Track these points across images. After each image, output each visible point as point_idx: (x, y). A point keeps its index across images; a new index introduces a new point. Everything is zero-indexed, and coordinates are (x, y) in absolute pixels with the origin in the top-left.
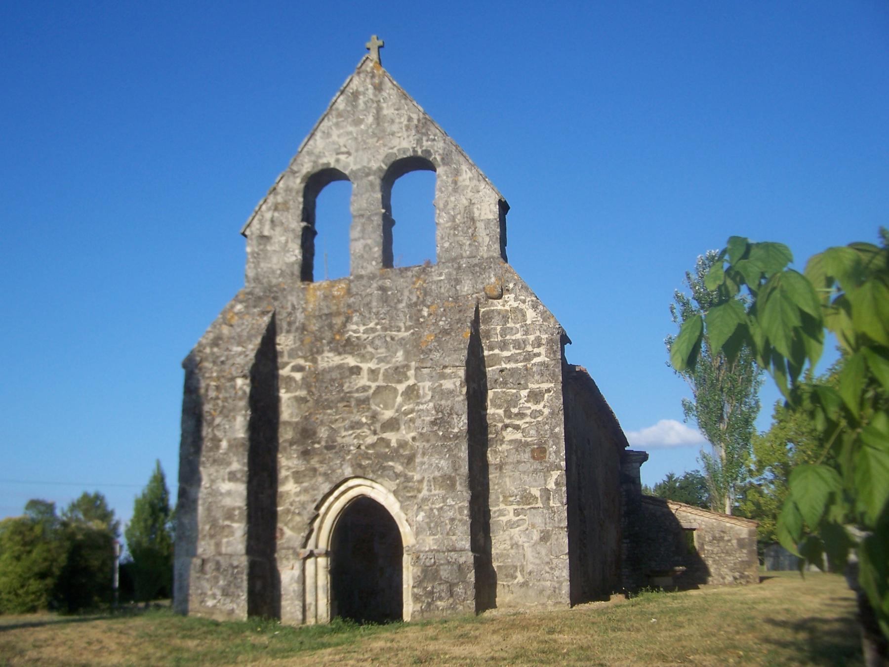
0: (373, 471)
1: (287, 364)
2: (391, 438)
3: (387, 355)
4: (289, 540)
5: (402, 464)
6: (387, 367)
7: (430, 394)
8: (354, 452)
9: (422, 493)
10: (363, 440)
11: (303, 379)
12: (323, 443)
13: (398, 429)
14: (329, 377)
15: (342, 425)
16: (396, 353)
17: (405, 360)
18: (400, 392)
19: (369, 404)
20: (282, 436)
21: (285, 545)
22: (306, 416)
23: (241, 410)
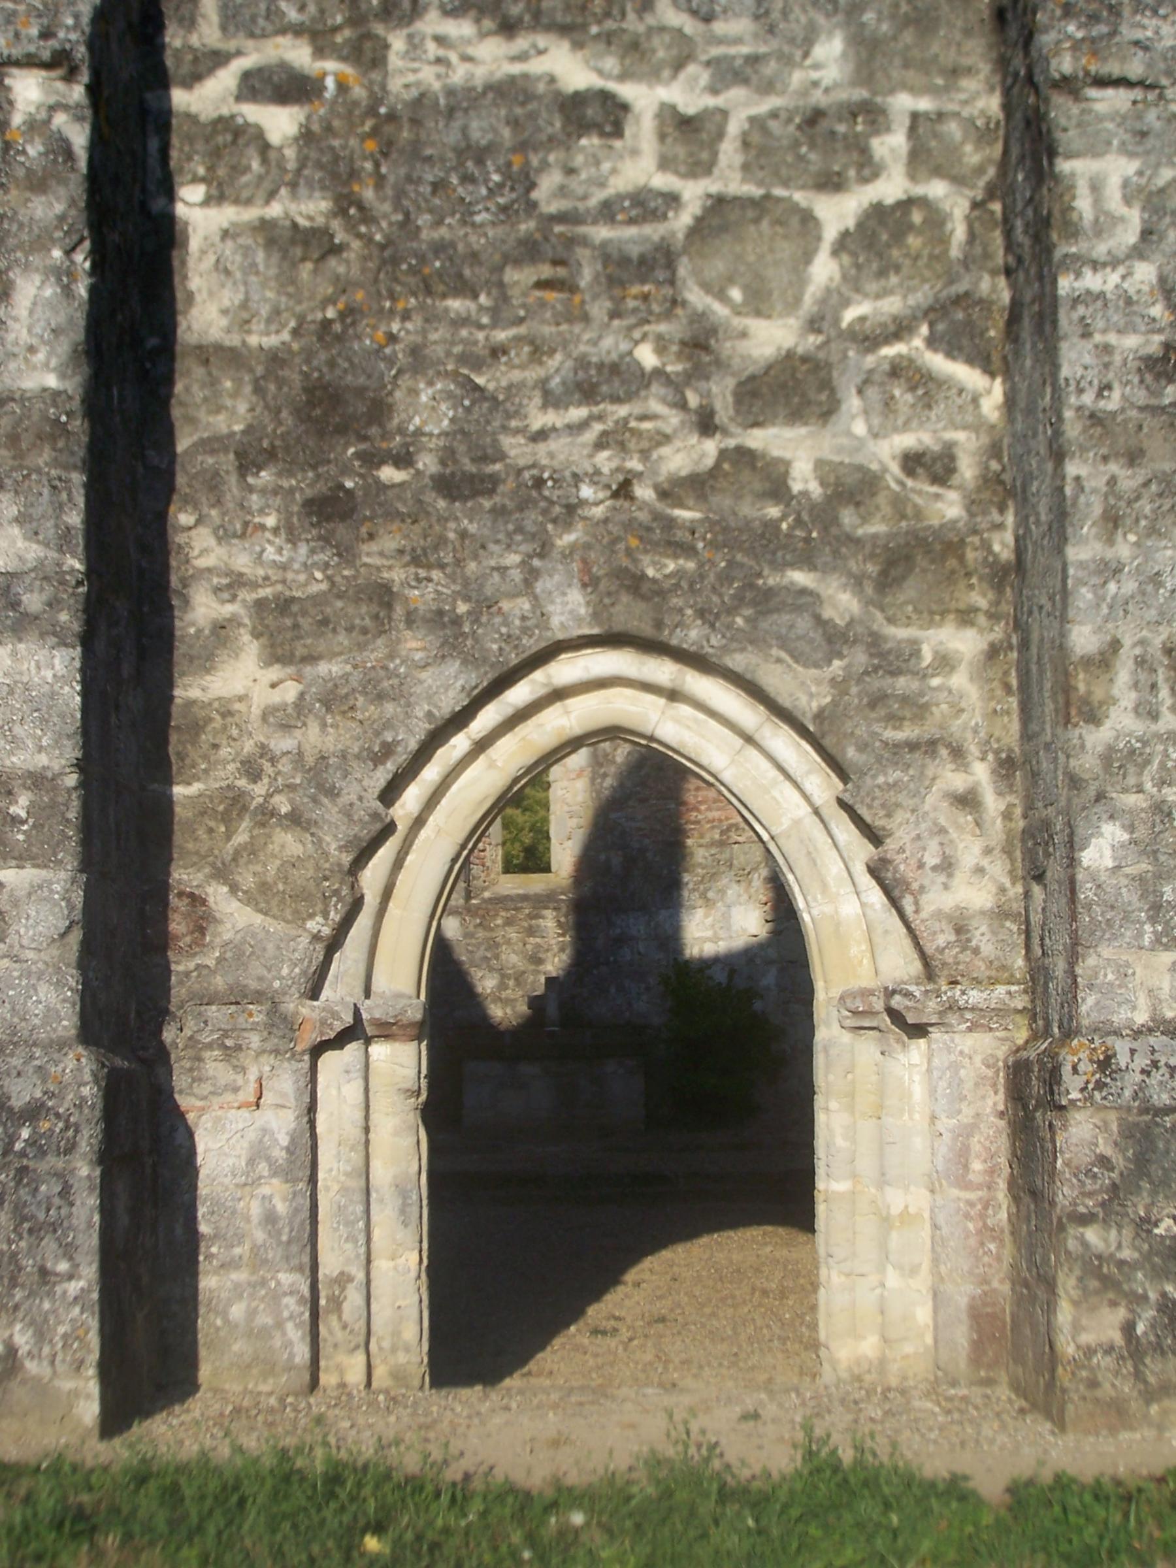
0: (701, 613)
1: (219, 59)
2: (787, 455)
3: (763, 49)
4: (238, 954)
5: (857, 582)
6: (763, 107)
7: (1134, 218)
8: (598, 512)
9: (1108, 724)
10: (645, 455)
11: (306, 136)
12: (428, 463)
13: (828, 412)
14: (452, 137)
15: (533, 374)
16: (808, 42)
17: (855, 82)
18: (830, 233)
19: (672, 282)
20: (192, 421)
21: (219, 982)
22: (326, 324)
23: (41, 244)
